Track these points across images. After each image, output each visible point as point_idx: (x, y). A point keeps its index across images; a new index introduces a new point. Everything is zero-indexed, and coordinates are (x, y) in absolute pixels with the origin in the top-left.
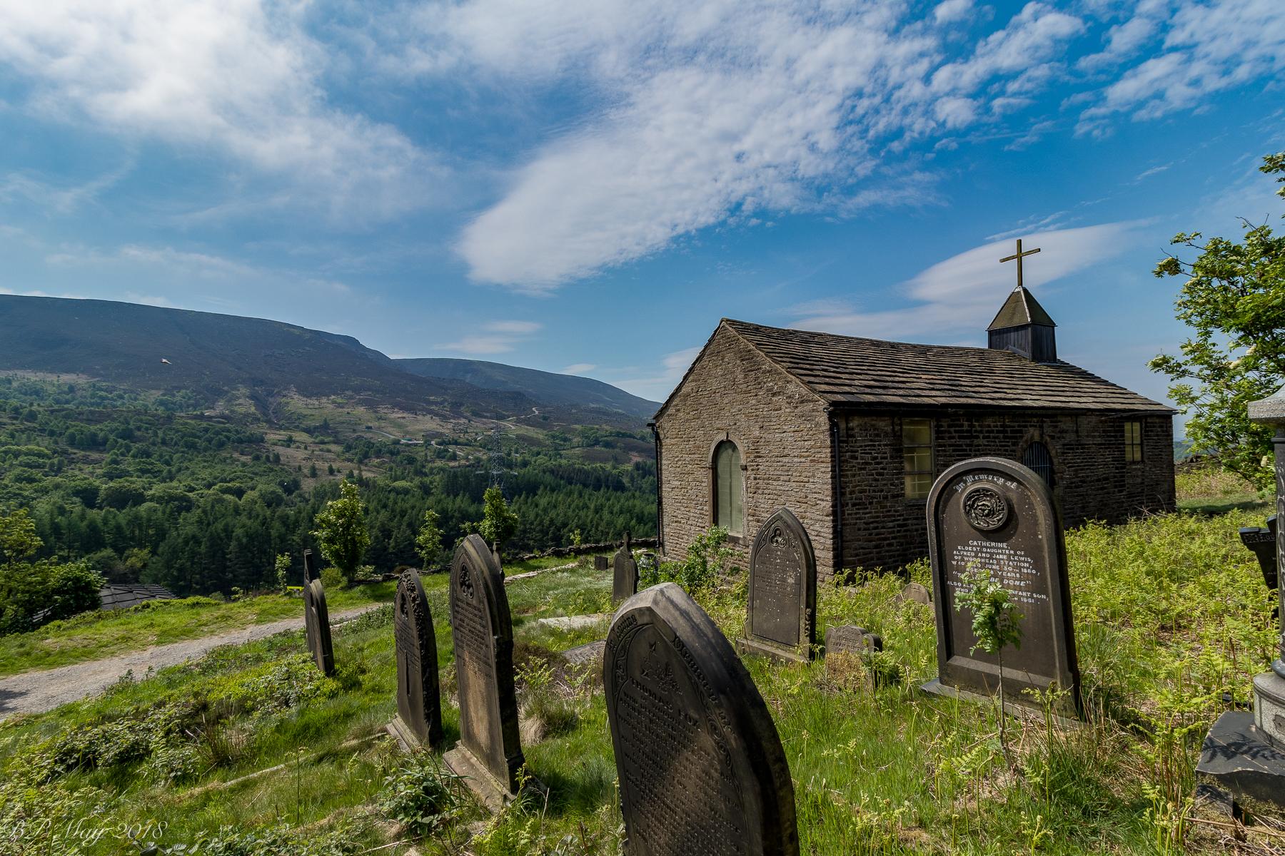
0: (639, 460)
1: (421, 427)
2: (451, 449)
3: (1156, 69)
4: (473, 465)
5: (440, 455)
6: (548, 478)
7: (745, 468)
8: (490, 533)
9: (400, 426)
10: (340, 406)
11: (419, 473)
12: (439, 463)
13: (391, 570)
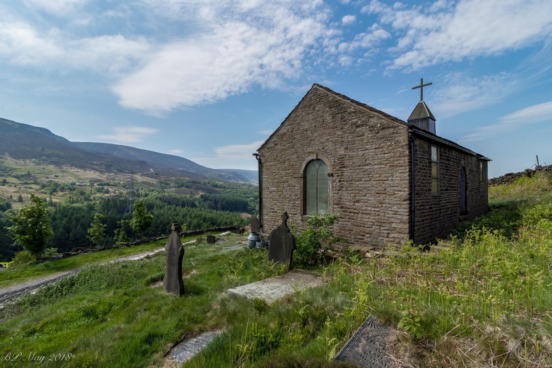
0: (203, 194)
1: (89, 176)
2: (106, 187)
3: (410, 55)
4: (118, 196)
5: (99, 191)
6: (158, 202)
7: (331, 175)
8: (136, 226)
9: (76, 176)
10: (38, 164)
11: (87, 199)
12: (98, 195)
13: (70, 249)
